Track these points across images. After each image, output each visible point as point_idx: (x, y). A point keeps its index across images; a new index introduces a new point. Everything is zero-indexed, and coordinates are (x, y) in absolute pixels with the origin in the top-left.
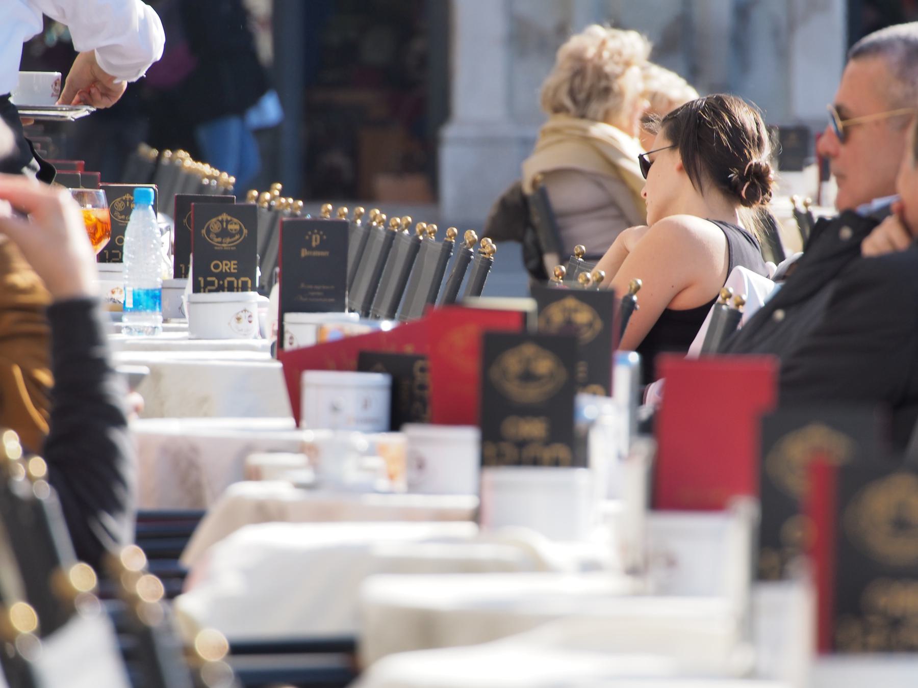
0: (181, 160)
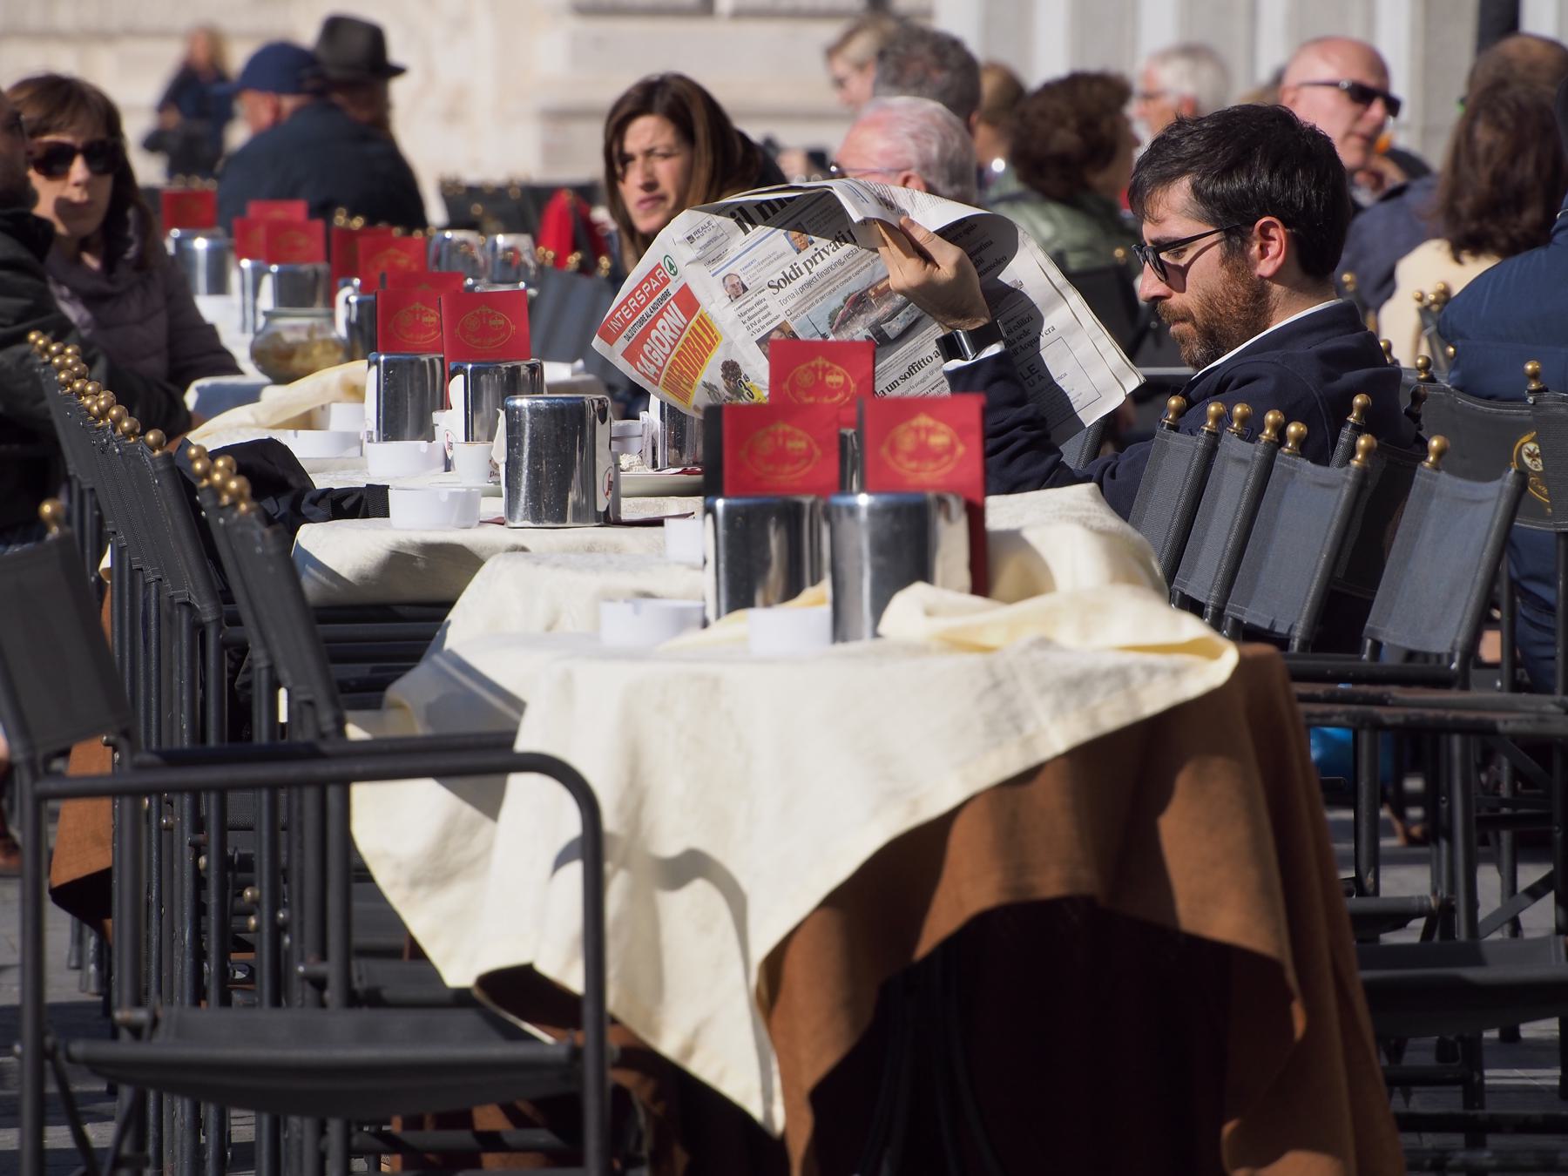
0: (512, 253)
